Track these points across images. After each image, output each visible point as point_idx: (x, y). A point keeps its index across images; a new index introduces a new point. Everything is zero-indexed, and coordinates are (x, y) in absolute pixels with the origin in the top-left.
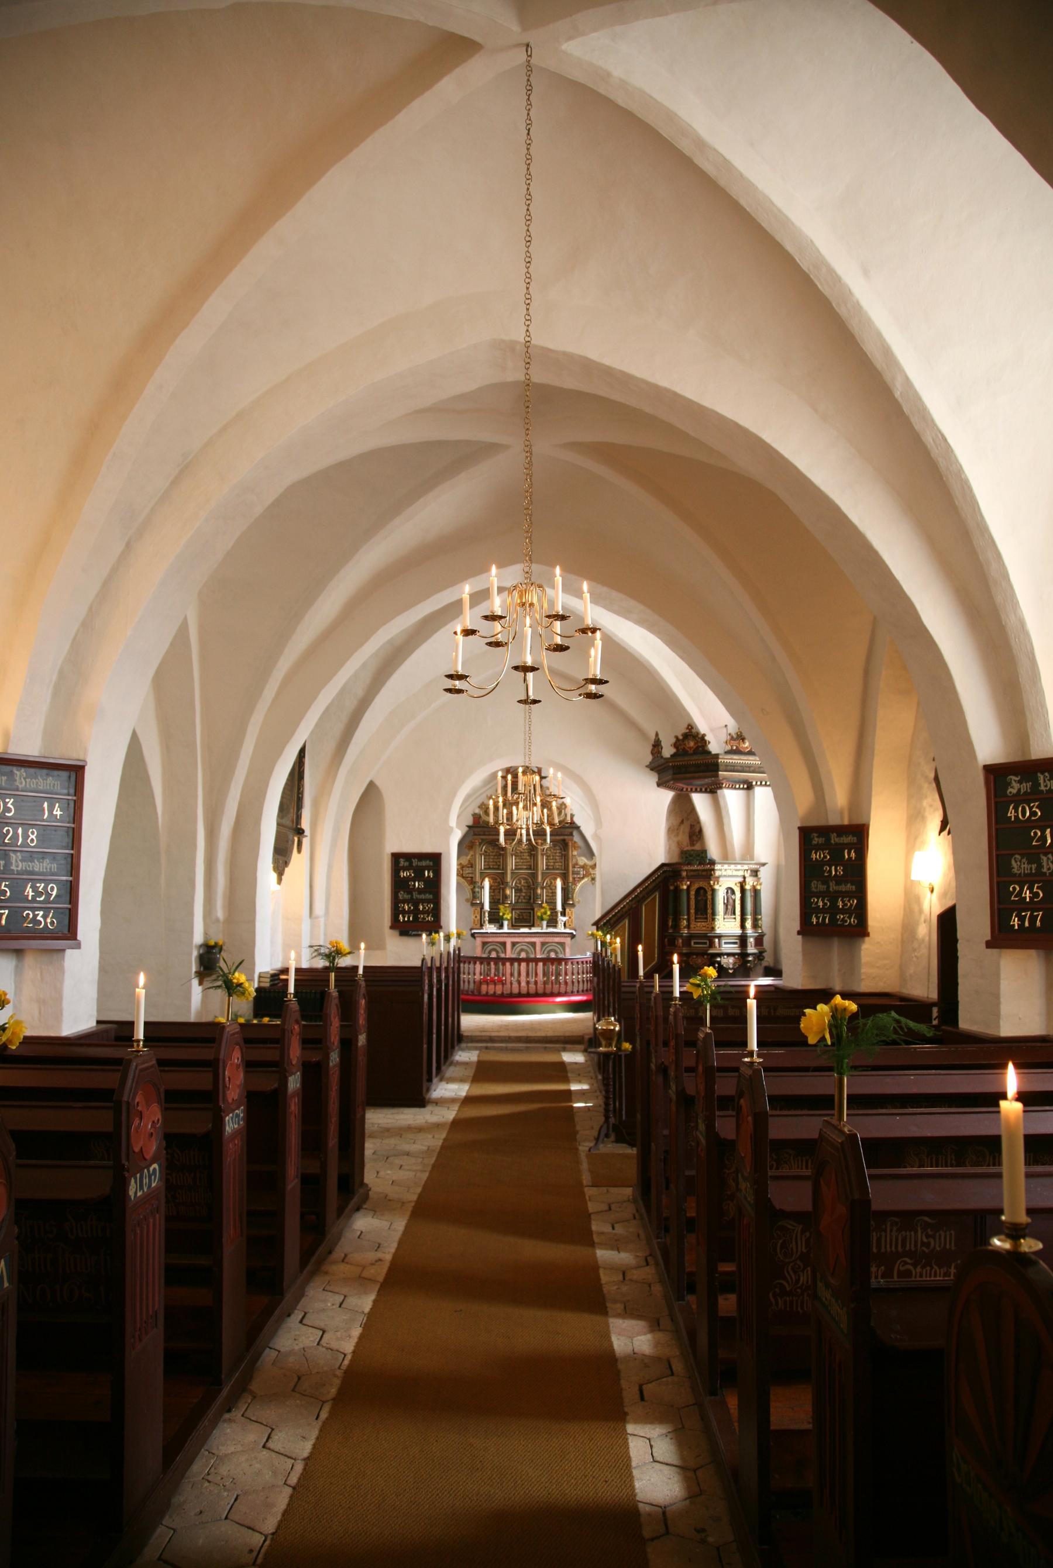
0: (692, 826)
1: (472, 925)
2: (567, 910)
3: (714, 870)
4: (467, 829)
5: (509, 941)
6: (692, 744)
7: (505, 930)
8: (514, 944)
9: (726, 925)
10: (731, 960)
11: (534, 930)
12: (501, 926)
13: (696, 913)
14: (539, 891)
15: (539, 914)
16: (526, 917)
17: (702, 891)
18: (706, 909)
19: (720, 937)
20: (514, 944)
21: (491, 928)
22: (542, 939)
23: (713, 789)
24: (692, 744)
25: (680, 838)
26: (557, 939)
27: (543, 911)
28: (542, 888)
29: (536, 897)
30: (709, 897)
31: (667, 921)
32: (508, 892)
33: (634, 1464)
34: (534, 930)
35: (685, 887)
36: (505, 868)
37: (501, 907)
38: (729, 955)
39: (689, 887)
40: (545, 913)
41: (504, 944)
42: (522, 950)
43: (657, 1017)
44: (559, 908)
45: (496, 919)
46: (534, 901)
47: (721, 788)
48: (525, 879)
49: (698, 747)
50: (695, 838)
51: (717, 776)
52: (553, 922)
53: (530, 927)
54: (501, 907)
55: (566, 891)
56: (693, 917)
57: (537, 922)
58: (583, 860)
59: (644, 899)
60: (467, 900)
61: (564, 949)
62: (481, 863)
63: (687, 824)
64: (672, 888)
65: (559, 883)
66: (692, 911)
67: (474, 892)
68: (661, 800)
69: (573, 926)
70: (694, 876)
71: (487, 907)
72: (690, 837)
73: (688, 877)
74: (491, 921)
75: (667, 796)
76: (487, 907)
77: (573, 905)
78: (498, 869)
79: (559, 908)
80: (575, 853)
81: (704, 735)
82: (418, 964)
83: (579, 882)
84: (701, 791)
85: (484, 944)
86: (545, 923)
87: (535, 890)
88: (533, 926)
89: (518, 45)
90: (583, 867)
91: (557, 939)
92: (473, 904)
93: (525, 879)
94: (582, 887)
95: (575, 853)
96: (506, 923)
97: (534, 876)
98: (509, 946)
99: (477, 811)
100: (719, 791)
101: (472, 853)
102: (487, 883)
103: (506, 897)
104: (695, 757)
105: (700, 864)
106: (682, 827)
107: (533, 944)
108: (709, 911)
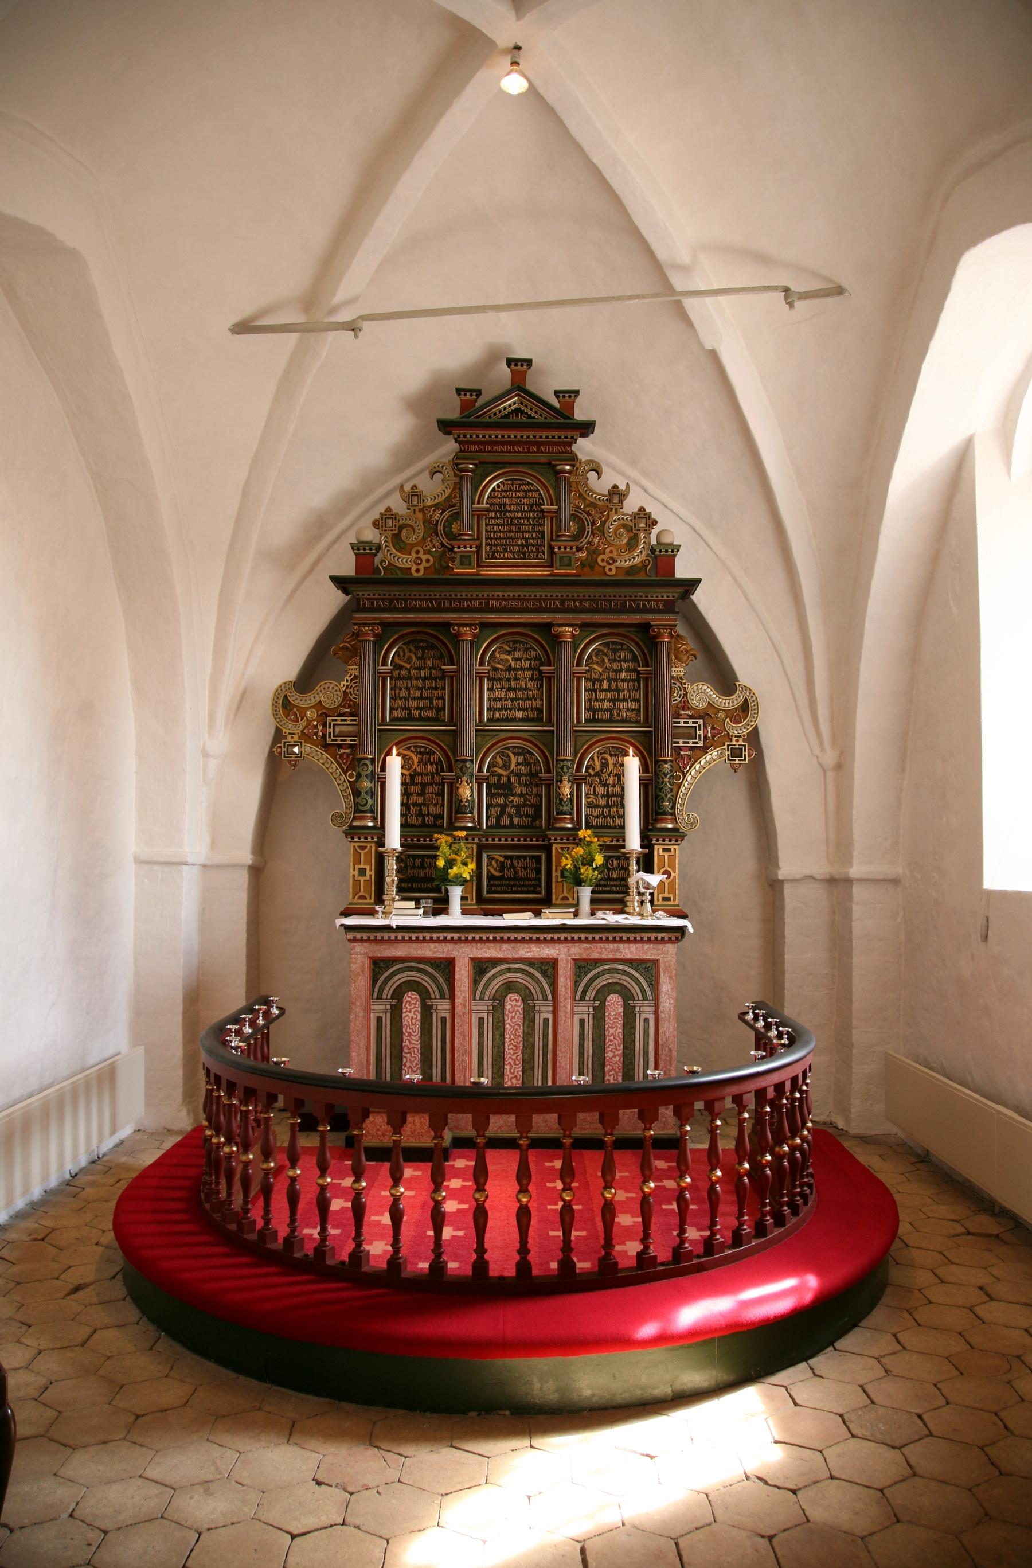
1: (348, 899)
2: (658, 850)
4: (335, 599)
5: (463, 955)
7: (455, 917)
8: (480, 967)
11: (550, 918)
12: (441, 906)
14: (566, 790)
15: (567, 863)
16: (522, 877)
20: (480, 967)
21: (404, 913)
22: (577, 951)
26: (630, 951)
27: (580, 853)
28: (577, 782)
29: (555, 808)
32: (466, 792)
33: (854, 917)
34: (550, 918)
36: (456, 718)
37: (443, 840)
40: (589, 861)
41: (447, 966)
42: (509, 987)
43: (838, 885)
44: (633, 842)
45: (423, 882)
46: (550, 826)
48: (522, 752)
52: (612, 891)
53: (536, 908)
54: (443, 840)
55: (651, 789)
57: (560, 889)
58: (703, 694)
60: (337, 819)
61: (655, 985)
62: (381, 705)
65: (632, 765)
67: (357, 793)
69: (677, 901)
71: (394, 839)
74: (405, 890)
76: (394, 839)
77: (677, 835)
78: (436, 720)
79: (633, 842)
80: (678, 671)
83: (694, 759)
85: (379, 966)
86: (586, 893)
87: (552, 786)
88: (547, 902)
89: (775, 288)
90: (706, 715)
91: (630, 951)
92: (352, 832)
93: (522, 752)
94: (708, 775)
95: (678, 671)
96: (456, 893)
97: (550, 742)
98: (463, 974)
99: (370, 535)
101: (353, 670)
102: (395, 764)
103: (458, 808)
107: (549, 967)
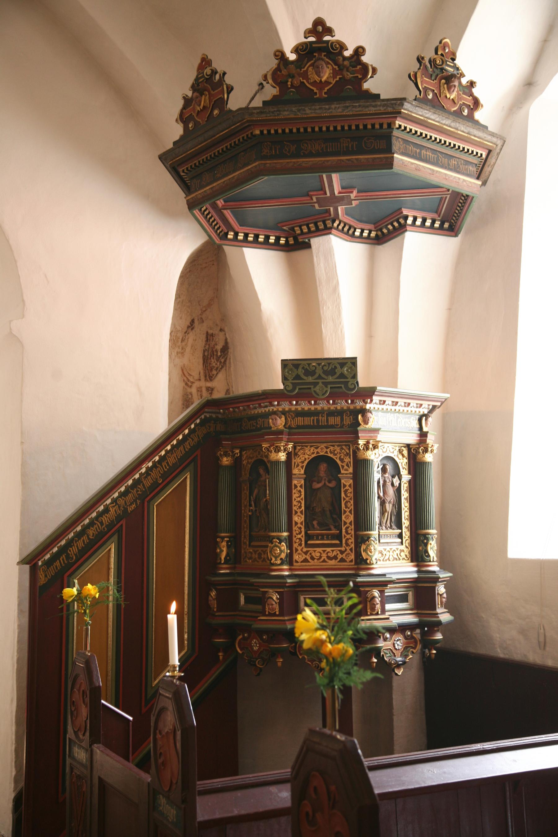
0: (209, 337)
3: (364, 412)
6: (326, 74)
9: (389, 557)
10: (399, 642)
13: (308, 525)
17: (323, 467)
18: (336, 512)
19: (382, 585)
23: (294, 239)
24: (326, 74)
25: (185, 361)
30: (347, 482)
31: (216, 545)
35: (282, 456)
38: (392, 630)
39: (237, 461)
47: (327, 230)
49: (343, 82)
50: (214, 362)
51: (389, 164)
56: (299, 536)
59: (156, 489)
63: (200, 330)
64: (226, 461)
66: (299, 519)
68: (166, 248)
70: (305, 428)
72: (206, 360)
73: (291, 432)
75: (176, 244)
81: (359, 51)
82: (363, 382)
84: (266, 244)
100: (315, 242)
104: (336, 109)
105: (335, 396)
106: (191, 336)
108: (348, 518)
